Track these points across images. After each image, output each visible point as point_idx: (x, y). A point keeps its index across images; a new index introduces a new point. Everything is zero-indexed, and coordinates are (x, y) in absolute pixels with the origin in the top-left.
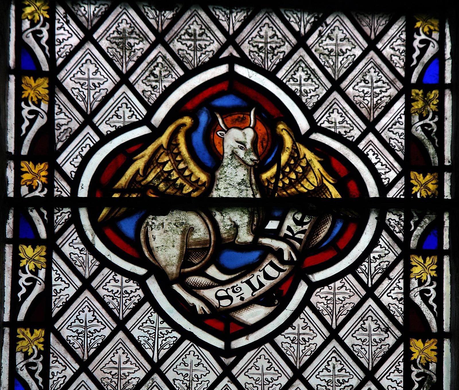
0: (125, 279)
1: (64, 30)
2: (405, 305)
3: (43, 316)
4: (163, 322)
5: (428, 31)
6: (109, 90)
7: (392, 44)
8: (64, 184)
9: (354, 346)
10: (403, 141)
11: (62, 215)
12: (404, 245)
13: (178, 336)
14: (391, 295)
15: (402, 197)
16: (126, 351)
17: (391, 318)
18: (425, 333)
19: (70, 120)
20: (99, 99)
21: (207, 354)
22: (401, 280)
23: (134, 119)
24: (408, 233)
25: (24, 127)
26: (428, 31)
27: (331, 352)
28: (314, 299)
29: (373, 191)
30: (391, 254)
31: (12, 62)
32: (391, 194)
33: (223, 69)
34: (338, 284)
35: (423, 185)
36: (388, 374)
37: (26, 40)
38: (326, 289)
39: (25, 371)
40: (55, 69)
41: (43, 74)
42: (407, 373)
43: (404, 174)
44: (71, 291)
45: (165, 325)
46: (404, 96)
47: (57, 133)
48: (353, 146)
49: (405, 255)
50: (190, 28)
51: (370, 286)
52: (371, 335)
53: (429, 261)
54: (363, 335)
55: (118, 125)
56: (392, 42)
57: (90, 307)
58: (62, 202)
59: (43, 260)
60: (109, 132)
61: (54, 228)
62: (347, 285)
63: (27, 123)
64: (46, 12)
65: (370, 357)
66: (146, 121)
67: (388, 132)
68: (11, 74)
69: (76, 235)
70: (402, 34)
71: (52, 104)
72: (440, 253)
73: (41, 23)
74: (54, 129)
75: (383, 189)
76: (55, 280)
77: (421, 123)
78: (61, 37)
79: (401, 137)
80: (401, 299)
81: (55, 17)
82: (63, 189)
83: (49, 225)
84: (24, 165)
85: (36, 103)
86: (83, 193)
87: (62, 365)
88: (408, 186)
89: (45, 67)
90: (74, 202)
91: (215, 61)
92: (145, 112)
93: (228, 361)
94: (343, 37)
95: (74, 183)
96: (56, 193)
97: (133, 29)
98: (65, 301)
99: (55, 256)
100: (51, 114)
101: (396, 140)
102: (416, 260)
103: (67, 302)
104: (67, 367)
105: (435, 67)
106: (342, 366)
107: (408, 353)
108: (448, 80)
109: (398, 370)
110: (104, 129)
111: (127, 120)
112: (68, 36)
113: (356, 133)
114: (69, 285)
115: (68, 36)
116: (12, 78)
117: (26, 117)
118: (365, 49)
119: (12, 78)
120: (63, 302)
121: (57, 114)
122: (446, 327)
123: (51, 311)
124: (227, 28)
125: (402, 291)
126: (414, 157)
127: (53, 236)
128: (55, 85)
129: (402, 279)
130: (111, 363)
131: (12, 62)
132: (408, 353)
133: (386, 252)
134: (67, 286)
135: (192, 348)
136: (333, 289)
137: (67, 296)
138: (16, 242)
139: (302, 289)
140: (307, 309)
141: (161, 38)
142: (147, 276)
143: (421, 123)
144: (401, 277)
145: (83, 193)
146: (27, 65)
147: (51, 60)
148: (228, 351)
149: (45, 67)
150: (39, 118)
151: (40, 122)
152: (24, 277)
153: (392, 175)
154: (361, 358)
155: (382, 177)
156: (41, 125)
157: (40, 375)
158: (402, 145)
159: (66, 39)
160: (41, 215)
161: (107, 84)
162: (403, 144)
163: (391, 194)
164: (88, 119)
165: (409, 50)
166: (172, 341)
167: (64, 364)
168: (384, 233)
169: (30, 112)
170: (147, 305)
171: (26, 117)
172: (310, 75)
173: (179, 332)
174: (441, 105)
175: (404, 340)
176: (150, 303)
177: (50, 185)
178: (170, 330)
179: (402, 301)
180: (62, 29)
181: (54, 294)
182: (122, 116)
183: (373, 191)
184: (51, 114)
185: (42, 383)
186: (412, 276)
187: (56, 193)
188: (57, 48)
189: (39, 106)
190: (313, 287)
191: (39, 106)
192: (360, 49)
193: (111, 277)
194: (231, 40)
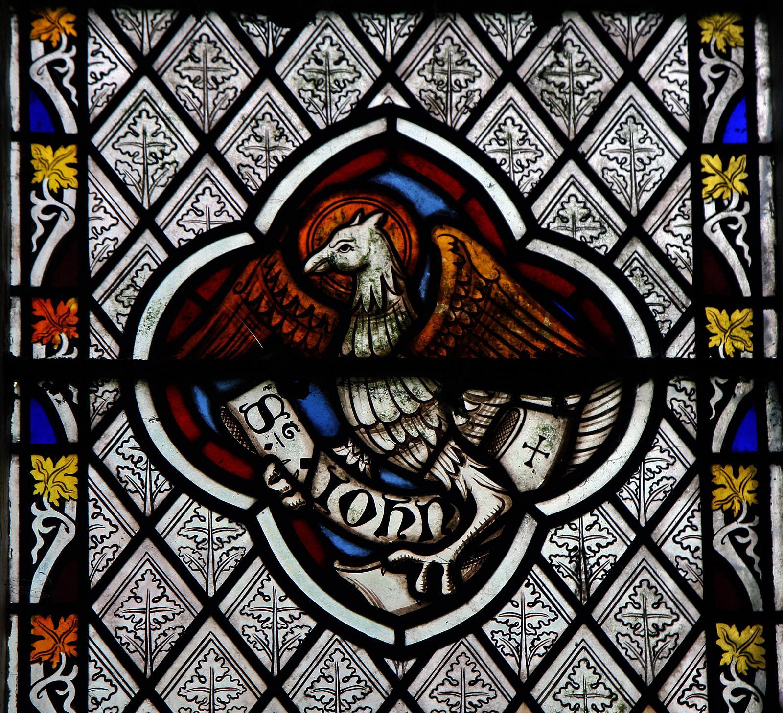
0: (215, 516)
1: (104, 56)
2: (694, 247)
3: (75, 590)
4: (286, 597)
5: (725, 47)
6: (181, 165)
7: (668, 225)
8: (109, 340)
9: (606, 171)
10: (690, 250)
11: (105, 394)
12: (699, 444)
13: (313, 624)
14: (681, 542)
15: (692, 357)
16: (223, 658)
17: (682, 583)
18: (731, 300)
19: (114, 66)
20: (163, 181)
21: (363, 655)
22: (695, 513)
23: (224, 218)
24: (706, 425)
25: (34, 553)
26: (725, 47)
27: (568, 184)
28: (547, 549)
29: (643, 349)
30: (678, 464)
31: (15, 125)
32: (672, 352)
33: (377, 127)
34: (588, 519)
35: (728, 332)
36: (680, 694)
37: (36, 79)
38: (566, 530)
39: (47, 74)
40: (88, 126)
41: (67, 140)
42: (695, 65)
43: (694, 313)
44: (121, 233)
45: (289, 603)
46: (697, 478)
47: (92, 244)
48: (605, 263)
49: (701, 470)
50: (319, 50)
51: (643, 524)
52: (650, 609)
53: (744, 473)
54: (621, 151)
55: (197, 227)
56: (667, 220)
57: (154, 572)
58: (103, 371)
59: (71, 173)
60: (183, 243)
61: (89, 421)
62: (601, 520)
63: (40, 230)
64: (71, 26)
65: (649, 659)
66: (246, 224)
67: (664, 233)
68: (14, 140)
69: (130, 432)
70: (699, 675)
71: (82, 502)
72: (752, 149)
73: (62, 667)
74: (86, 240)
75: (659, 342)
76: (93, 211)
77: (720, 216)
78: (98, 224)
79: (687, 242)
80: (685, 83)
81: (88, 495)
82: (103, 345)
83: (81, 412)
84: (40, 308)
85: (57, 504)
86: (141, 349)
87: (111, 216)
88: (702, 335)
89: (70, 125)
90: (124, 371)
91: (361, 114)
92: (243, 206)
93: (400, 670)
94: (595, 681)
95: (126, 339)
96: (93, 354)
97: (222, 205)
98: (112, 249)
99: (92, 473)
100: (81, 210)
101: (678, 247)
102: (711, 162)
103: (115, 251)
104: (120, 689)
105: (741, 109)
106: (582, 56)
107: (713, 654)
108: (763, 132)
109: (679, 61)
110: (176, 235)
111: (213, 218)
112: (110, 68)
113: (610, 240)
114: (118, 529)
115: (110, 68)
116: (15, 145)
117: (39, 219)
118: (619, 80)
119: (15, 145)
120: (110, 252)
121: (93, 517)
122: (768, 289)
123: (87, 579)
124: (381, 50)
125: (699, 533)
126: (709, 282)
127: (90, 434)
128: (87, 151)
129: (698, 511)
130: (196, 519)
131: (15, 125)
132: (713, 654)
133: (670, 459)
134: (114, 221)
135: (336, 645)
136: (582, 687)
137: (115, 548)
138: (26, 139)
139: (265, 220)
140: (536, 569)
141: (267, 69)
142: (256, 509)
143: (720, 216)
144: (695, 507)
145: (141, 349)
146: (41, 125)
147: (80, 112)
148: (400, 651)
149: (70, 125)
150: (61, 221)
151: (64, 226)
152: (40, 204)
153: (674, 315)
154: (632, 659)
155: (657, 319)
156: (64, 233)
157: (72, 82)
158: (688, 257)
159: (106, 72)
160: (68, 397)
161: (175, 155)
162: (691, 256)
163: (672, 352)
164: (147, 219)
165: (696, 85)
166: (303, 633)
167: (114, 214)
168: (665, 426)
169: (47, 522)
170: (258, 563)
171: (39, 219)
172: (527, 134)
173: (314, 617)
174: (752, 182)
175: (704, 626)
176: (263, 560)
177: (82, 342)
178: (296, 614)
179: (689, 242)
180: (100, 55)
181: (91, 235)
182: (201, 57)
183: (643, 349)
184: (81, 210)
185: (77, 98)
186: (714, 507)
187: (93, 354)
188: (91, 89)
189: (61, 509)
190: (246, 224)
191: (61, 509)
192: (622, 543)
193: (190, 513)
194: (390, 73)
